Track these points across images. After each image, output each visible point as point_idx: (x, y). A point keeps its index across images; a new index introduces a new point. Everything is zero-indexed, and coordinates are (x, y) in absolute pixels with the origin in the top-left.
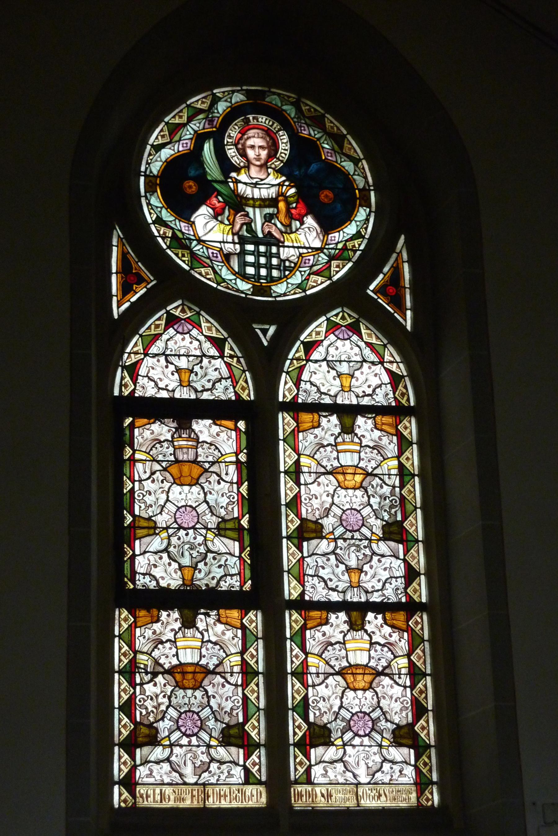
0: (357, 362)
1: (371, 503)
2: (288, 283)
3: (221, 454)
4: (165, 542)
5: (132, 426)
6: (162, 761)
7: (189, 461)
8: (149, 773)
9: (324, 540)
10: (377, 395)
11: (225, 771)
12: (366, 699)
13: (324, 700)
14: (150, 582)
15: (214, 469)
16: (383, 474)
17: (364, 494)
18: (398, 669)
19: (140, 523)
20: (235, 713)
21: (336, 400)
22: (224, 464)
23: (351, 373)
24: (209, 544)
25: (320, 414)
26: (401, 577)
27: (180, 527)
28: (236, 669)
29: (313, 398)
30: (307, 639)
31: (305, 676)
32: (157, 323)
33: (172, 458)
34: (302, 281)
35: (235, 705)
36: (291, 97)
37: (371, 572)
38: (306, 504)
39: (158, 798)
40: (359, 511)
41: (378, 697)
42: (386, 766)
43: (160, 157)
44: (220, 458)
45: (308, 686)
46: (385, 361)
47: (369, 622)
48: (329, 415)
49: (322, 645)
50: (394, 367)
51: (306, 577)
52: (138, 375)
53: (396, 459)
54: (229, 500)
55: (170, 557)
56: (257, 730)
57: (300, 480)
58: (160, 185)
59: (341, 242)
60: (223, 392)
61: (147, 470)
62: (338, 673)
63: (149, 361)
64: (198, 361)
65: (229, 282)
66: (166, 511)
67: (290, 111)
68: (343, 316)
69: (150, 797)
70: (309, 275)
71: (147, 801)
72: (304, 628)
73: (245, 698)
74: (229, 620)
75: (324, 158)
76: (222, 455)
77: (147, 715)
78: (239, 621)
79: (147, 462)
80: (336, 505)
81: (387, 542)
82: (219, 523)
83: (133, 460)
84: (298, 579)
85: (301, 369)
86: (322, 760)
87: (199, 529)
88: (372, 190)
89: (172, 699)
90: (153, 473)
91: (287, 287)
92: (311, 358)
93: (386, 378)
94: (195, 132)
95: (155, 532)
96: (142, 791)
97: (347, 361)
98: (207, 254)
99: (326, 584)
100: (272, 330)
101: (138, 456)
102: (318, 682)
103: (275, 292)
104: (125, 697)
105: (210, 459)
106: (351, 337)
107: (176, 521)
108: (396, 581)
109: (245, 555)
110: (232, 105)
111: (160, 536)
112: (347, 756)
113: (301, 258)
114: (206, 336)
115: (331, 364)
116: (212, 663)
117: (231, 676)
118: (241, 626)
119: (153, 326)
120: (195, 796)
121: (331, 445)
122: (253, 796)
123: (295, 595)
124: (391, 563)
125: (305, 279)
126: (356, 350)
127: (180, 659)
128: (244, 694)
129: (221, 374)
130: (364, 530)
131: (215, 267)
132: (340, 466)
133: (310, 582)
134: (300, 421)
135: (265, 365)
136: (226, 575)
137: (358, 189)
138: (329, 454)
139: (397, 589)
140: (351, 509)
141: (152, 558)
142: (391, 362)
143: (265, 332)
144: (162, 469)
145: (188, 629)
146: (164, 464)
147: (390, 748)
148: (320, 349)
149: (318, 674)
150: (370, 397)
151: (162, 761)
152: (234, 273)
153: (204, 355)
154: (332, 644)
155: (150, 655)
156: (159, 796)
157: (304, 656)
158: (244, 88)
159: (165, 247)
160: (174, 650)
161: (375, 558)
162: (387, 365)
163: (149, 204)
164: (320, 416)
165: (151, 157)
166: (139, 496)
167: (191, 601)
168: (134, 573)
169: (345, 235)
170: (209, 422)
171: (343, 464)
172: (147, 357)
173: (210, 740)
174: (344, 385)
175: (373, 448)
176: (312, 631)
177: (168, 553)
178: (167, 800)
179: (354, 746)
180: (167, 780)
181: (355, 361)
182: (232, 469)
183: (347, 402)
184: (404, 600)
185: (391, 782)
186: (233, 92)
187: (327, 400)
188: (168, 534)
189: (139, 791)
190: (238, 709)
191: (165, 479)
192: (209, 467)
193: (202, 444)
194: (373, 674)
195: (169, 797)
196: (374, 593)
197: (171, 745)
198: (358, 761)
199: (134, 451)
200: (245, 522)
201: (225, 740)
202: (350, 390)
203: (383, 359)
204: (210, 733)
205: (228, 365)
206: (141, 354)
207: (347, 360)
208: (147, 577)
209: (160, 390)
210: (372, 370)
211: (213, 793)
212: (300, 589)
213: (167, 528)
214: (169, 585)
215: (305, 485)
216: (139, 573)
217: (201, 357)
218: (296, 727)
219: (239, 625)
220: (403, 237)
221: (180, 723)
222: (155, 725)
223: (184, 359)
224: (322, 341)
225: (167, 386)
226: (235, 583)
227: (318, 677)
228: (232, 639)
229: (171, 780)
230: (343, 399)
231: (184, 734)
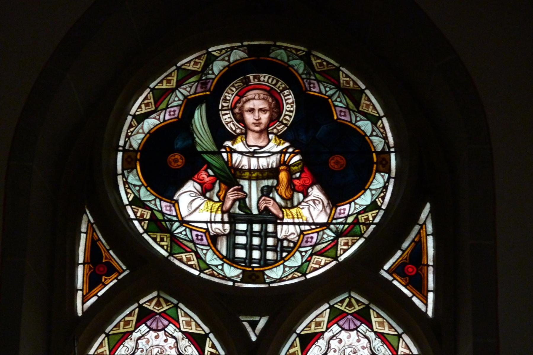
34: (302, 264)
36: (300, 50)
43: (142, 128)
58: (140, 160)
65: (214, 268)
67: (299, 66)
70: (311, 255)
100: (262, 322)
103: (269, 277)
113: (302, 236)
125: (306, 261)
131: (199, 251)
152: (221, 257)
158: (245, 43)
159: (141, 231)
163: (126, 183)
169: (357, 206)
186: (232, 49)
220: (428, 206)
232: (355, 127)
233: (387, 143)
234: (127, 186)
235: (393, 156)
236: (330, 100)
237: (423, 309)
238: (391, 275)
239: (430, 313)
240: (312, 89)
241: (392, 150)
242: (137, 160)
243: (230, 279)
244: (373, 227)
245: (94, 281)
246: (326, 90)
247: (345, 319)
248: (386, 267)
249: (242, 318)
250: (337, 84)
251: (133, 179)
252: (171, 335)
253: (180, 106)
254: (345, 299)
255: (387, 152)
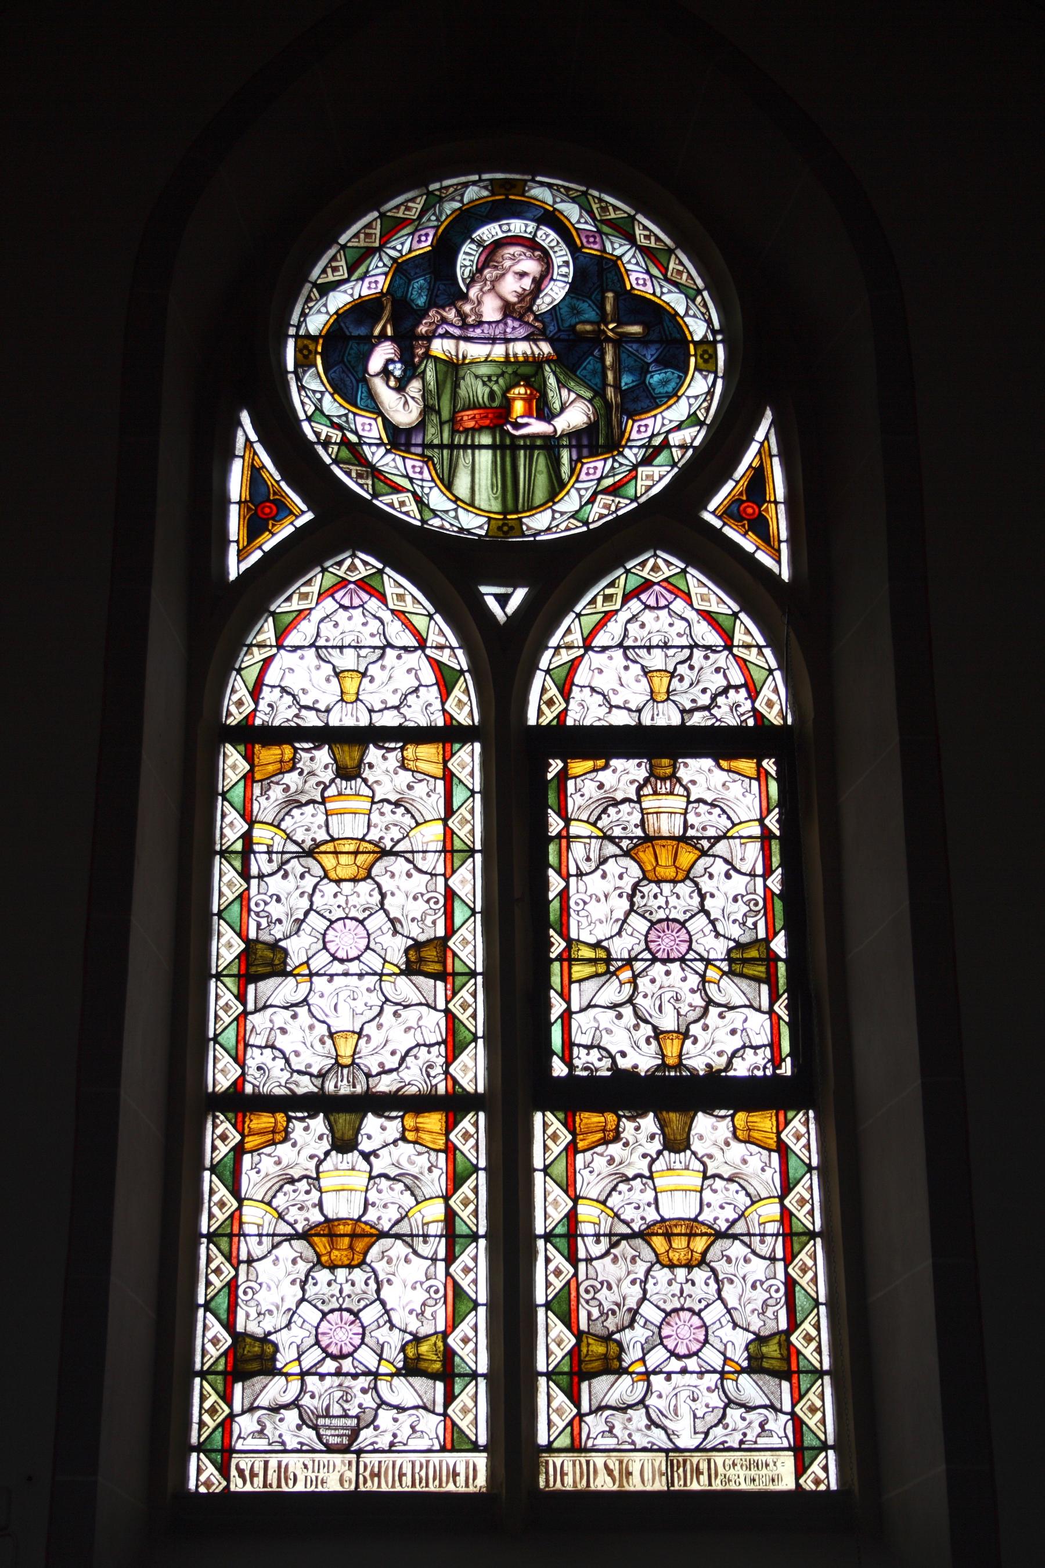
0: (375, 648)
1: (706, 908)
2: (554, 511)
3: (732, 822)
4: (628, 989)
5: (563, 776)
6: (286, 1407)
7: (672, 838)
8: (259, 1428)
9: (290, 978)
10: (409, 706)
11: (756, 1425)
12: (353, 1284)
13: (609, 1287)
14: (600, 1060)
15: (721, 848)
16: (412, 852)
17: (693, 892)
18: (760, 1224)
19: (580, 953)
20: (428, 1312)
21: (639, 719)
22: (737, 841)
23: (362, 670)
24: (712, 989)
25: (297, 745)
26: (765, 1046)
27: (654, 960)
28: (772, 1228)
29: (284, 715)
30: (244, 1170)
31: (235, 1239)
32: (608, 591)
33: (639, 832)
34: (581, 507)
35: (430, 1297)
36: (572, 189)
37: (703, 1037)
38: (257, 914)
39: (272, 1477)
40: (361, 922)
41: (717, 1281)
42: (734, 1415)
44: (729, 830)
45: (240, 1262)
46: (736, 643)
47: (701, 1137)
48: (316, 748)
49: (277, 1179)
50: (445, 657)
51: (575, 1049)
52: (573, 684)
53: (440, 822)
54: (748, 908)
55: (637, 1015)
56: (473, 1346)
57: (249, 869)
58: (321, 354)
59: (658, 434)
60: (424, 711)
61: (592, 856)
62: (298, 1236)
63: (284, 659)
64: (375, 657)
65: (565, 198)
66: (630, 930)
67: (571, 212)
68: (353, 563)
69: (567, 1474)
70: (595, 494)
71: (252, 1483)
72: (239, 1151)
73: (790, 1284)
74: (754, 1134)
75: (628, 287)
76: (734, 825)
77: (603, 1318)
78: (774, 1136)
79: (594, 841)
80: (318, 913)
81: (413, 978)
82: (729, 951)
83: (566, 838)
84: (233, 1052)
85: (574, 665)
86: (603, 1404)
87: (691, 960)
88: (720, 342)
89: (306, 1287)
90: (603, 861)
91: (554, 518)
92: (285, 644)
93: (428, 676)
94: (620, 258)
95: (608, 968)
96: (242, 1466)
97: (355, 647)
98: (627, 462)
99: (287, 1061)
100: (519, 596)
101: (575, 829)
102: (598, 1254)
103: (529, 528)
104: (558, 1284)
105: (711, 832)
106: (670, 603)
107: (647, 948)
108: (429, 1052)
109: (781, 1009)
110: (464, 205)
111: (618, 977)
112: (655, 1395)
113: (579, 465)
114: (698, 611)
115: (323, 652)
116: (722, 1219)
117: (425, 1242)
118: (777, 1146)
119: (600, 599)
120: (405, 1475)
121: (630, 800)
122: (702, 1473)
123: (224, 1083)
124: (745, 1020)
125: (587, 503)
126: (374, 625)
127: (325, 1212)
128: (787, 1275)
129: (418, 679)
130: (368, 956)
132: (329, 838)
133: (254, 1058)
134: (256, 761)
135: (502, 659)
136: (744, 1047)
137: (693, 341)
138: (626, 818)
139: (431, 1067)
140: (667, 919)
141: (282, 1017)
142: (440, 647)
143: (503, 597)
144: (621, 853)
145: (676, 1152)
146: (625, 844)
147: (396, 1380)
148: (304, 625)
149: (597, 1236)
150: (706, 713)
151: (286, 1407)
152: (453, 499)
153: (390, 645)
154: (626, 1180)
155: (604, 1203)
156: (276, 1475)
157: (235, 1205)
158: (485, 176)
160: (650, 1195)
161: (714, 1011)
162: (428, 651)
164: (296, 750)
165: (310, 305)
166: (577, 904)
167: (675, 1095)
168: (568, 1044)
170: (708, 763)
171: (336, 836)
172: (590, 653)
173: (379, 1365)
174: (656, 690)
175: (397, 804)
176: (588, 1154)
177: (634, 1006)
178: (291, 1483)
179: (322, 1376)
180: (641, 1441)
181: (370, 647)
182: (754, 849)
183: (661, 722)
184: (441, 1089)
185: (743, 1446)
186: (466, 185)
187: (311, 720)
188: (633, 972)
189: (237, 1465)
190: (777, 1304)
191: (309, 872)
192: (710, 848)
193: (695, 805)
194: (709, 1235)
195: (295, 1476)
196: (383, 1076)
197: (647, 1374)
198: (676, 1406)
199: (568, 821)
200: (779, 945)
201: (754, 1364)
202: (668, 699)
203: (732, 639)
204: (379, 1352)
205: (743, 664)
206: (579, 647)
207: (353, 644)
208: (595, 1052)
209: (614, 709)
210: (710, 662)
211: (709, 1468)
212: (235, 1072)
213: (629, 962)
214: (636, 1066)
215: (577, 875)
216: (579, 1045)
217: (383, 648)
218: (552, 1342)
219: (772, 1143)
220: (769, 415)
221: (665, 1332)
222: (616, 1336)
223: (350, 653)
224: (616, 612)
225: (626, 702)
226: (434, 1059)
227: (598, 1242)
228: (761, 1170)
229: (300, 1443)
230: (341, 718)
231: (673, 1354)
232: (661, 303)
233: (299, 379)
234: (303, 393)
235: (720, 348)
236: (619, 262)
237: (776, 570)
238: (720, 517)
239: (785, 576)
240: (592, 246)
241: (719, 337)
242: (317, 353)
243: (542, 184)
244: (690, 452)
245: (255, 528)
246: (618, 248)
247: (650, 591)
248: (712, 507)
249: (484, 589)
250: (631, 239)
251: (312, 383)
252: (374, 616)
253: (386, 274)
254: (647, 560)
255: (708, 342)
